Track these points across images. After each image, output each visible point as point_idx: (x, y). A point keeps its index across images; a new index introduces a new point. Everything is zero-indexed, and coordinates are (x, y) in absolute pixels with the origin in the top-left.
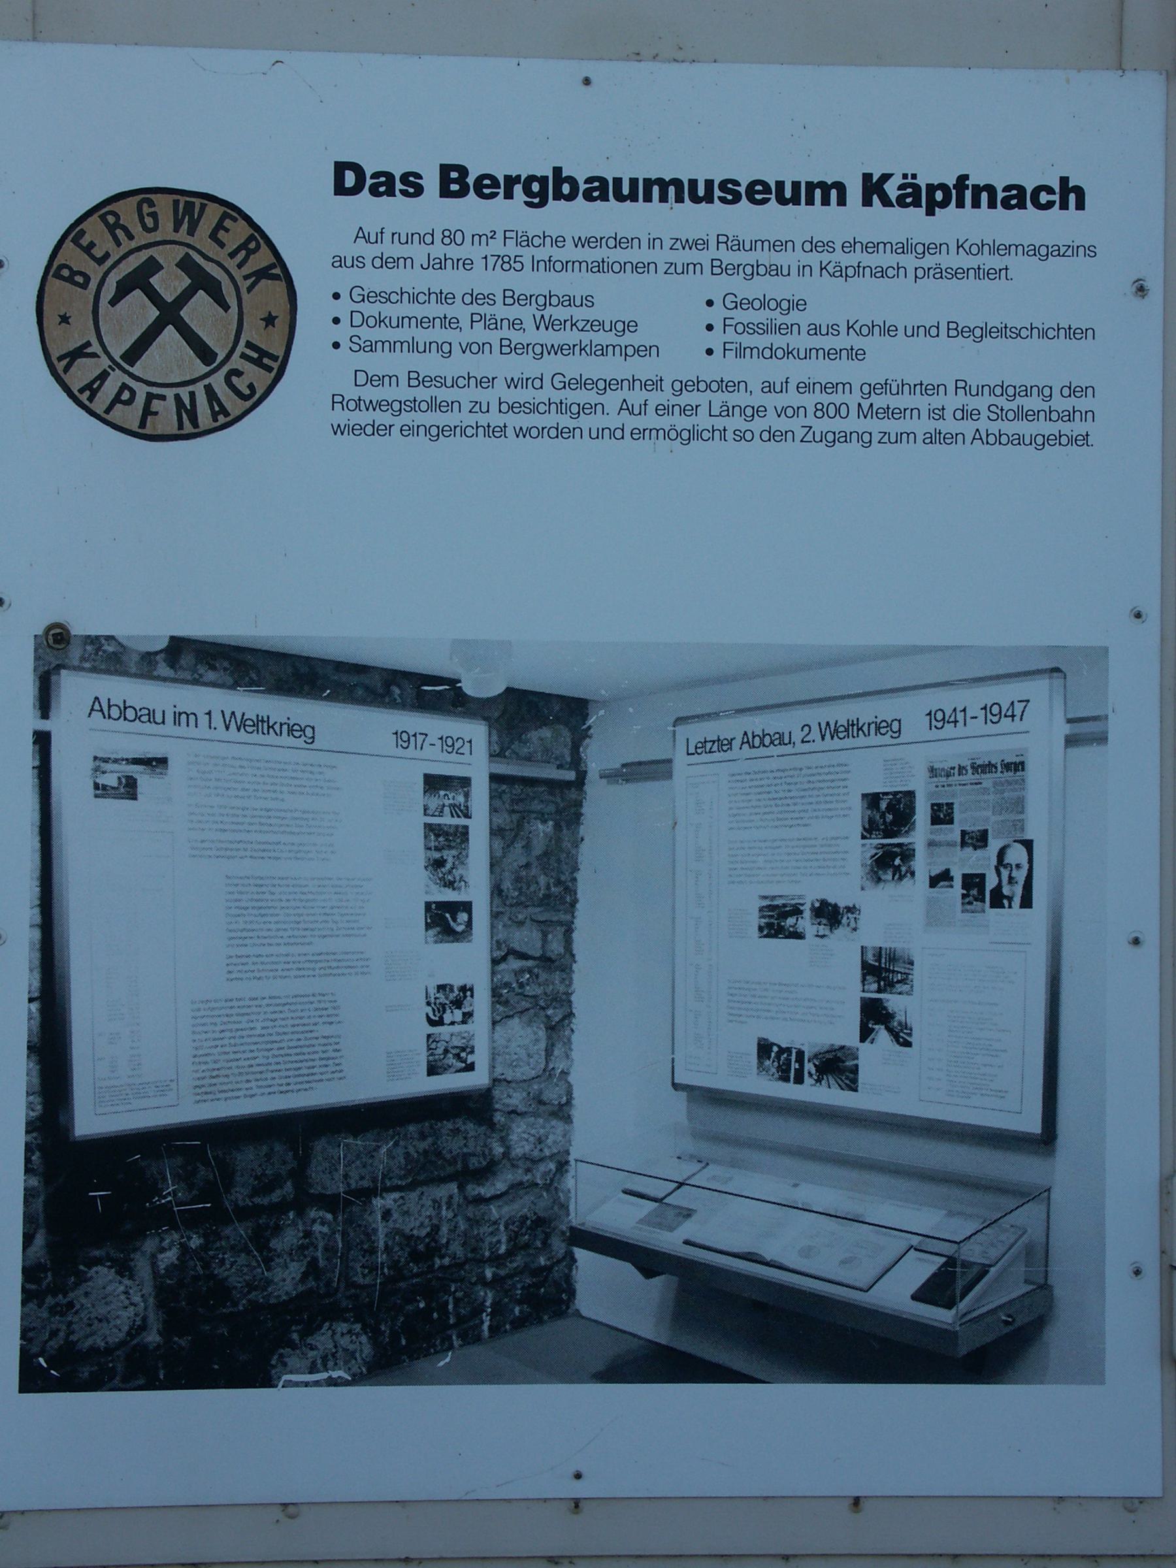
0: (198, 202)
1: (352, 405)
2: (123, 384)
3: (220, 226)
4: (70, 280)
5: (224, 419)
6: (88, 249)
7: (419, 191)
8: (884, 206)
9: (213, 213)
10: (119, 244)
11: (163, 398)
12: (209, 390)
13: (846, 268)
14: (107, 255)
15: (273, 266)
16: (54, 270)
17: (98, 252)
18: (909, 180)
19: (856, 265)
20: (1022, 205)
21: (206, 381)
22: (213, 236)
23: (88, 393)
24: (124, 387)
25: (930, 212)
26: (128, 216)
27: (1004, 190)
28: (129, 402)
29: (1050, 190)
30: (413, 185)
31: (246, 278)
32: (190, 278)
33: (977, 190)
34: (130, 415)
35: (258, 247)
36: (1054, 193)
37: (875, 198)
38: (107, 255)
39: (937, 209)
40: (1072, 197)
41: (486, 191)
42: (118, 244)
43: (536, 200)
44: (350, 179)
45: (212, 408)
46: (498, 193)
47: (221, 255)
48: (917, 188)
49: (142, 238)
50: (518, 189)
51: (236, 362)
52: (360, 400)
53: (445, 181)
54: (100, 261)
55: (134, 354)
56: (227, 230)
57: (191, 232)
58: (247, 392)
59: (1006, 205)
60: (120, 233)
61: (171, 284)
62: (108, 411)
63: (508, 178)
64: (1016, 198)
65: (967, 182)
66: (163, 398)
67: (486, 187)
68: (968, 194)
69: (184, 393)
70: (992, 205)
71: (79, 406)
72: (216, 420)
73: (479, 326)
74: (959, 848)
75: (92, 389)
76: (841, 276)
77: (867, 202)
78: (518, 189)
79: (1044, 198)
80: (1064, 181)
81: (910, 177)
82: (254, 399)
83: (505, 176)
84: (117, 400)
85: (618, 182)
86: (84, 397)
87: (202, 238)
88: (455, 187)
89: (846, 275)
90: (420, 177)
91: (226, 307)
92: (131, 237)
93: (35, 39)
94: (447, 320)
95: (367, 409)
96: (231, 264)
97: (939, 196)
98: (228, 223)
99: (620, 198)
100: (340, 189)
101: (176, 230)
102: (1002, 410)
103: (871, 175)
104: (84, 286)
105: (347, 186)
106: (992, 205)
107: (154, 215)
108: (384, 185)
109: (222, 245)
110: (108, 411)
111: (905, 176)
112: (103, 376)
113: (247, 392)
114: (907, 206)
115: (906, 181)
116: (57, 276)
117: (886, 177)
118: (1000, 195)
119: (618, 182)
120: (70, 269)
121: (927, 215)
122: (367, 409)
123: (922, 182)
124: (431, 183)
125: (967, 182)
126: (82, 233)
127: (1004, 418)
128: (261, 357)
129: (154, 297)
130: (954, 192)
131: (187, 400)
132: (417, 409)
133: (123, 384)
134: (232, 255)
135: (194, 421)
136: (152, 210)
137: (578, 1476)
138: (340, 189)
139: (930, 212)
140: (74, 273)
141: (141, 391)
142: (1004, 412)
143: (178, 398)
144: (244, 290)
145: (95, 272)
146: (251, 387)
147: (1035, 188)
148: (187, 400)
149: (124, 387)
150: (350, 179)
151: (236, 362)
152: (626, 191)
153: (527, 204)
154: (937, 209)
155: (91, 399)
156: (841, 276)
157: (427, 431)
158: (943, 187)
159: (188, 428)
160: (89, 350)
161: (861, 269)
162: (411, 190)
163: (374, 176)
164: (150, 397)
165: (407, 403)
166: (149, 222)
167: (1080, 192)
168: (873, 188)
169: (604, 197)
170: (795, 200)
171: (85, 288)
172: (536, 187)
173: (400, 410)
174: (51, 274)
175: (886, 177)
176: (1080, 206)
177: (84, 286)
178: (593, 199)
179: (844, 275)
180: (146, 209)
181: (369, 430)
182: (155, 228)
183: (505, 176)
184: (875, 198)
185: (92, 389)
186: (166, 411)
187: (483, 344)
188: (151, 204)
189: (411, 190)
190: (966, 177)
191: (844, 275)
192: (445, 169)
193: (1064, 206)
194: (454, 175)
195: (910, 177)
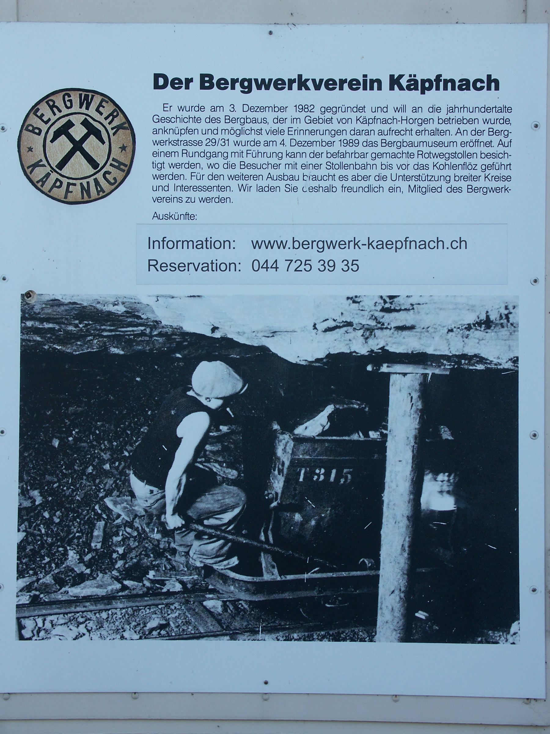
0: (90, 95)
1: (427, 156)
2: (57, 179)
3: (100, 105)
4: (33, 131)
5: (103, 194)
6: (41, 117)
8: (400, 90)
9: (97, 100)
10: (55, 114)
11: (75, 185)
12: (96, 180)
14: (49, 120)
15: (124, 123)
16: (25, 127)
17: (45, 118)
18: (413, 78)
20: (468, 89)
21: (94, 177)
22: (97, 110)
23: (41, 183)
24: (57, 180)
25: (423, 93)
26: (59, 103)
28: (60, 187)
29: (482, 81)
31: (112, 129)
32: (87, 129)
33: (446, 82)
34: (60, 192)
35: (118, 115)
36: (484, 82)
38: (49, 120)
39: (426, 91)
40: (493, 84)
42: (55, 114)
43: (246, 90)
44: (161, 81)
45: (97, 189)
47: (101, 119)
48: (416, 81)
49: (65, 111)
50: (237, 85)
51: (108, 168)
52: (430, 153)
53: (202, 82)
54: (46, 122)
55: (62, 164)
56: (104, 107)
57: (87, 108)
58: (113, 181)
59: (460, 88)
60: (55, 110)
61: (78, 132)
62: (50, 191)
63: (232, 80)
64: (465, 85)
65: (441, 78)
66: (75, 185)
67: (222, 84)
68: (442, 84)
69: (84, 182)
70: (453, 89)
71: (37, 189)
72: (98, 194)
75: (43, 181)
76: (366, 123)
77: (392, 88)
78: (237, 85)
79: (479, 85)
80: (489, 76)
81: (413, 76)
82: (117, 184)
83: (289, 79)
84: (54, 186)
86: (39, 185)
87: (92, 111)
88: (207, 84)
89: (369, 123)
91: (103, 143)
92: (60, 111)
93: (18, 21)
95: (434, 158)
96: (106, 123)
97: (427, 85)
98: (104, 104)
100: (157, 86)
101: (81, 107)
104: (39, 134)
105: (159, 85)
106: (453, 89)
107: (70, 101)
108: (176, 84)
109: (101, 114)
110: (50, 191)
111: (410, 76)
112: (48, 175)
113: (113, 181)
114: (411, 90)
115: (410, 78)
116: (27, 130)
117: (401, 76)
118: (457, 84)
120: (33, 126)
121: (421, 94)
122: (434, 158)
123: (419, 78)
125: (441, 78)
126: (38, 110)
128: (119, 165)
129: (71, 138)
130: (434, 83)
131: (85, 185)
132: (457, 157)
133: (57, 179)
134: (106, 118)
135: (89, 195)
136: (70, 98)
137: (266, 683)
138: (157, 86)
139: (423, 93)
140: (34, 128)
141: (65, 181)
143: (81, 184)
144: (111, 134)
145: (44, 128)
146: (115, 179)
148: (85, 185)
149: (57, 180)
150: (161, 81)
151: (108, 168)
153: (242, 92)
154: (426, 91)
155: (42, 186)
156: (366, 123)
158: (429, 81)
159: (86, 198)
160: (41, 163)
161: (376, 120)
163: (460, 81)
164: (69, 184)
165: (452, 154)
166: (68, 104)
167: (496, 82)
168: (395, 82)
171: (39, 135)
172: (246, 84)
173: (449, 157)
174: (24, 129)
175: (401, 76)
176: (497, 88)
177: (39, 134)
178: (463, 90)
179: (367, 122)
180: (67, 98)
182: (71, 107)
183: (340, 79)
185: (43, 181)
186: (76, 190)
188: (69, 96)
190: (441, 75)
191: (367, 122)
192: (203, 76)
193: (489, 89)
194: (207, 79)
195: (413, 76)
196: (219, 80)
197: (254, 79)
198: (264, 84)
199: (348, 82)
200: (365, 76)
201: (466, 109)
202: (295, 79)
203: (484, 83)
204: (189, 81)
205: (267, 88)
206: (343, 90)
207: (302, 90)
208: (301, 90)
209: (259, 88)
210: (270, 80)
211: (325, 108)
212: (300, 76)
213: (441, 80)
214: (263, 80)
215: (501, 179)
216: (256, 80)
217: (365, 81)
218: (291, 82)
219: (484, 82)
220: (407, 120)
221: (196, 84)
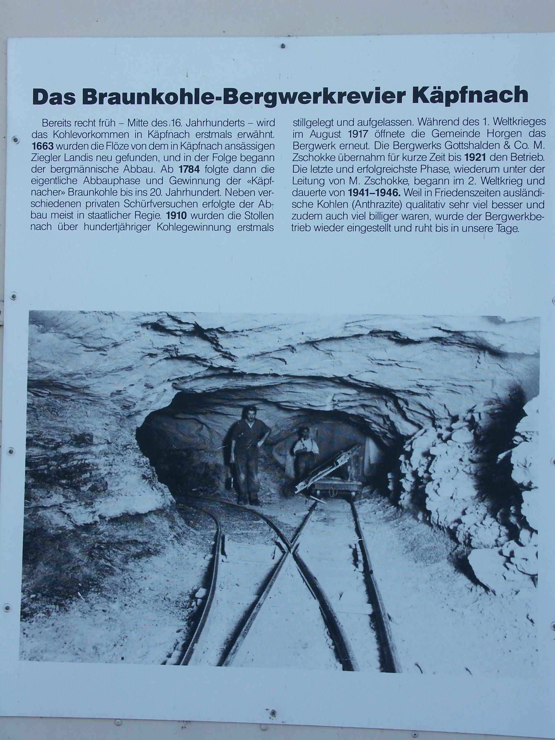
7: (73, 101)
8: (424, 102)
13: (161, 133)
18: (437, 90)
19: (165, 132)
20: (495, 100)
25: (447, 105)
27: (486, 93)
29: (509, 93)
30: (70, 99)
33: (472, 94)
36: (512, 94)
37: (419, 98)
40: (521, 96)
41: (246, 100)
43: (271, 104)
44: (40, 97)
46: (394, 100)
48: (441, 93)
50: (262, 99)
53: (85, 96)
59: (487, 100)
63: (257, 94)
64: (492, 97)
65: (466, 90)
67: (246, 98)
68: (467, 96)
70: (479, 100)
73: (425, 171)
74: (357, 569)
77: (415, 101)
79: (506, 96)
80: (517, 88)
81: (437, 88)
85: (125, 95)
90: (74, 95)
94: (517, 168)
97: (452, 97)
99: (126, 102)
100: (36, 101)
102: (252, 214)
103: (418, 87)
106: (479, 100)
108: (57, 99)
111: (435, 88)
114: (435, 102)
115: (435, 90)
117: (425, 89)
118: (484, 96)
119: (125, 95)
124: (79, 97)
125: (466, 90)
127: (253, 218)
130: (460, 95)
138: (36, 101)
139: (447, 105)
142: (253, 215)
147: (385, 92)
150: (40, 97)
152: (129, 99)
157: (360, 229)
158: (454, 93)
161: (168, 134)
162: (70, 101)
163: (52, 95)
167: (525, 93)
168: (418, 94)
169: (118, 102)
170: (132, 102)
172: (270, 98)
175: (425, 89)
176: (525, 100)
178: (55, 104)
181: (332, 228)
183: (398, 92)
184: (419, 98)
187: (341, 180)
189: (70, 101)
190: (466, 87)
192: (85, 91)
193: (517, 100)
194: (90, 93)
195: (437, 88)
196: (243, 95)
197: (279, 93)
198: (288, 98)
199: (347, 95)
200: (378, 88)
201: (208, 123)
202: (321, 92)
203: (512, 94)
204: (401, 94)
205: (292, 102)
206: (527, 102)
207: (156, 104)
208: (156, 103)
209: (284, 101)
210: (295, 94)
211: (376, 121)
212: (326, 90)
213: (467, 92)
214: (288, 94)
215: (67, 216)
216: (281, 94)
217: (378, 94)
218: (316, 95)
219: (512, 94)
220: (493, 133)
221: (408, 97)
